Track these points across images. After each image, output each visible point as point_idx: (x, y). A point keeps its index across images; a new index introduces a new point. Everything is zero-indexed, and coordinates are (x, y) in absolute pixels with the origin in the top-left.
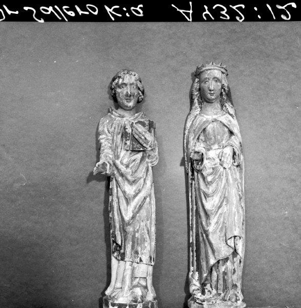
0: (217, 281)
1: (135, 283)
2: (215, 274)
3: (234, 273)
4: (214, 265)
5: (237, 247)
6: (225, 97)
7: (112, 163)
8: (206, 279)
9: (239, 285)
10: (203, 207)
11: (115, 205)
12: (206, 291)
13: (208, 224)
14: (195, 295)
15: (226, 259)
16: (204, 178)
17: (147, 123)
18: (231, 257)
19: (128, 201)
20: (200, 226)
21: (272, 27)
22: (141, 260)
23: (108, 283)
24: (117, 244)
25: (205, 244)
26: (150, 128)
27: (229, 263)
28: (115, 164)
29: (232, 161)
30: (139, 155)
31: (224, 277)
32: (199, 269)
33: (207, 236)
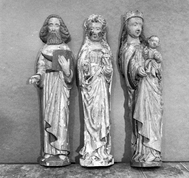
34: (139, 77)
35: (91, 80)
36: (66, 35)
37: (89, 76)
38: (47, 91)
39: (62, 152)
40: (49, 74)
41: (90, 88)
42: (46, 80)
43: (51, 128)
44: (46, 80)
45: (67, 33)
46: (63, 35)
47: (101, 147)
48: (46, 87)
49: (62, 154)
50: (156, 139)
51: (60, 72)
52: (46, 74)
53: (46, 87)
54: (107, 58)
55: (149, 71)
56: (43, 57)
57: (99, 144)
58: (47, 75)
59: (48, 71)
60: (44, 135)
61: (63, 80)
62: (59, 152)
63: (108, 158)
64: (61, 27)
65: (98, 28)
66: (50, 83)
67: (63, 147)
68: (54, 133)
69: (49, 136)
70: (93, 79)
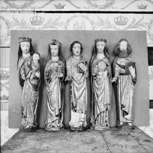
0: (101, 120)
1: (80, 120)
2: (99, 116)
3: (106, 117)
4: (99, 114)
5: (108, 108)
6: (106, 51)
7: (71, 77)
8: (96, 119)
9: (108, 121)
10: (96, 93)
11: (73, 92)
12: (96, 123)
13: (98, 99)
14: (92, 124)
15: (104, 112)
16: (97, 82)
17: (85, 62)
18: (105, 111)
19: (78, 91)
20: (95, 99)
21: (48, 51)
22: (82, 112)
23: (70, 120)
24: (73, 106)
25: (96, 106)
26: (86, 64)
27: (105, 113)
28: (72, 77)
29: (107, 76)
30: (82, 74)
31: (103, 118)
32: (94, 115)
33: (97, 104)
34: (24, 81)
35: (50, 81)
36: (130, 51)
37: (49, 79)
38: (122, 86)
39: (130, 121)
40: (122, 76)
41: (50, 86)
42: (120, 80)
43: (125, 108)
44: (120, 80)
45: (131, 50)
46: (128, 51)
47: (56, 120)
48: (120, 84)
49: (130, 123)
50: (30, 116)
51: (129, 75)
52: (120, 76)
53: (120, 84)
54: (60, 67)
55: (28, 76)
56: (118, 65)
57: (55, 118)
58: (121, 77)
59: (121, 74)
60: (118, 111)
61: (131, 80)
62: (128, 121)
63: (60, 126)
64: (128, 46)
65: (56, 49)
66: (123, 81)
67: (131, 119)
68: (127, 111)
69: (123, 112)
70: (52, 80)
